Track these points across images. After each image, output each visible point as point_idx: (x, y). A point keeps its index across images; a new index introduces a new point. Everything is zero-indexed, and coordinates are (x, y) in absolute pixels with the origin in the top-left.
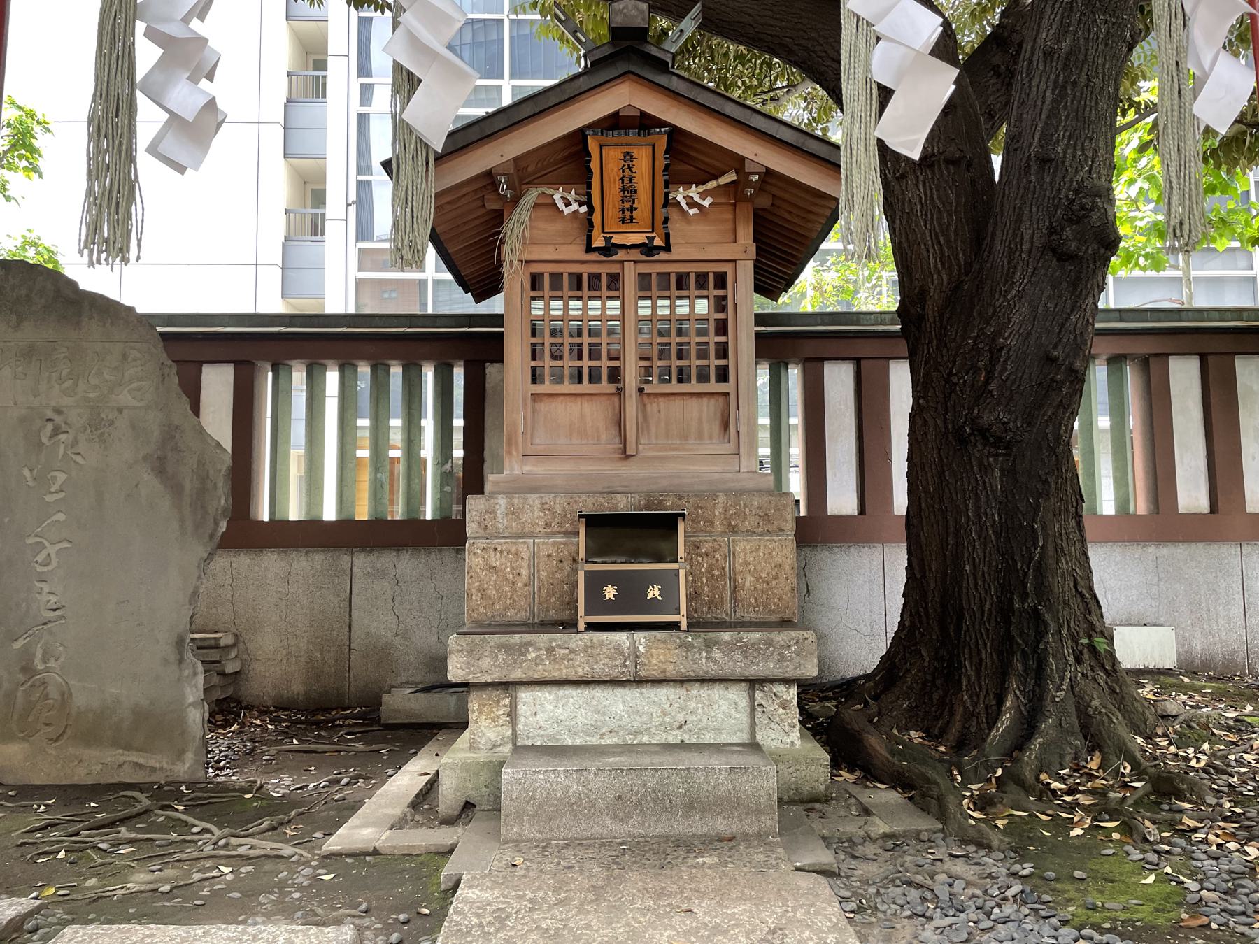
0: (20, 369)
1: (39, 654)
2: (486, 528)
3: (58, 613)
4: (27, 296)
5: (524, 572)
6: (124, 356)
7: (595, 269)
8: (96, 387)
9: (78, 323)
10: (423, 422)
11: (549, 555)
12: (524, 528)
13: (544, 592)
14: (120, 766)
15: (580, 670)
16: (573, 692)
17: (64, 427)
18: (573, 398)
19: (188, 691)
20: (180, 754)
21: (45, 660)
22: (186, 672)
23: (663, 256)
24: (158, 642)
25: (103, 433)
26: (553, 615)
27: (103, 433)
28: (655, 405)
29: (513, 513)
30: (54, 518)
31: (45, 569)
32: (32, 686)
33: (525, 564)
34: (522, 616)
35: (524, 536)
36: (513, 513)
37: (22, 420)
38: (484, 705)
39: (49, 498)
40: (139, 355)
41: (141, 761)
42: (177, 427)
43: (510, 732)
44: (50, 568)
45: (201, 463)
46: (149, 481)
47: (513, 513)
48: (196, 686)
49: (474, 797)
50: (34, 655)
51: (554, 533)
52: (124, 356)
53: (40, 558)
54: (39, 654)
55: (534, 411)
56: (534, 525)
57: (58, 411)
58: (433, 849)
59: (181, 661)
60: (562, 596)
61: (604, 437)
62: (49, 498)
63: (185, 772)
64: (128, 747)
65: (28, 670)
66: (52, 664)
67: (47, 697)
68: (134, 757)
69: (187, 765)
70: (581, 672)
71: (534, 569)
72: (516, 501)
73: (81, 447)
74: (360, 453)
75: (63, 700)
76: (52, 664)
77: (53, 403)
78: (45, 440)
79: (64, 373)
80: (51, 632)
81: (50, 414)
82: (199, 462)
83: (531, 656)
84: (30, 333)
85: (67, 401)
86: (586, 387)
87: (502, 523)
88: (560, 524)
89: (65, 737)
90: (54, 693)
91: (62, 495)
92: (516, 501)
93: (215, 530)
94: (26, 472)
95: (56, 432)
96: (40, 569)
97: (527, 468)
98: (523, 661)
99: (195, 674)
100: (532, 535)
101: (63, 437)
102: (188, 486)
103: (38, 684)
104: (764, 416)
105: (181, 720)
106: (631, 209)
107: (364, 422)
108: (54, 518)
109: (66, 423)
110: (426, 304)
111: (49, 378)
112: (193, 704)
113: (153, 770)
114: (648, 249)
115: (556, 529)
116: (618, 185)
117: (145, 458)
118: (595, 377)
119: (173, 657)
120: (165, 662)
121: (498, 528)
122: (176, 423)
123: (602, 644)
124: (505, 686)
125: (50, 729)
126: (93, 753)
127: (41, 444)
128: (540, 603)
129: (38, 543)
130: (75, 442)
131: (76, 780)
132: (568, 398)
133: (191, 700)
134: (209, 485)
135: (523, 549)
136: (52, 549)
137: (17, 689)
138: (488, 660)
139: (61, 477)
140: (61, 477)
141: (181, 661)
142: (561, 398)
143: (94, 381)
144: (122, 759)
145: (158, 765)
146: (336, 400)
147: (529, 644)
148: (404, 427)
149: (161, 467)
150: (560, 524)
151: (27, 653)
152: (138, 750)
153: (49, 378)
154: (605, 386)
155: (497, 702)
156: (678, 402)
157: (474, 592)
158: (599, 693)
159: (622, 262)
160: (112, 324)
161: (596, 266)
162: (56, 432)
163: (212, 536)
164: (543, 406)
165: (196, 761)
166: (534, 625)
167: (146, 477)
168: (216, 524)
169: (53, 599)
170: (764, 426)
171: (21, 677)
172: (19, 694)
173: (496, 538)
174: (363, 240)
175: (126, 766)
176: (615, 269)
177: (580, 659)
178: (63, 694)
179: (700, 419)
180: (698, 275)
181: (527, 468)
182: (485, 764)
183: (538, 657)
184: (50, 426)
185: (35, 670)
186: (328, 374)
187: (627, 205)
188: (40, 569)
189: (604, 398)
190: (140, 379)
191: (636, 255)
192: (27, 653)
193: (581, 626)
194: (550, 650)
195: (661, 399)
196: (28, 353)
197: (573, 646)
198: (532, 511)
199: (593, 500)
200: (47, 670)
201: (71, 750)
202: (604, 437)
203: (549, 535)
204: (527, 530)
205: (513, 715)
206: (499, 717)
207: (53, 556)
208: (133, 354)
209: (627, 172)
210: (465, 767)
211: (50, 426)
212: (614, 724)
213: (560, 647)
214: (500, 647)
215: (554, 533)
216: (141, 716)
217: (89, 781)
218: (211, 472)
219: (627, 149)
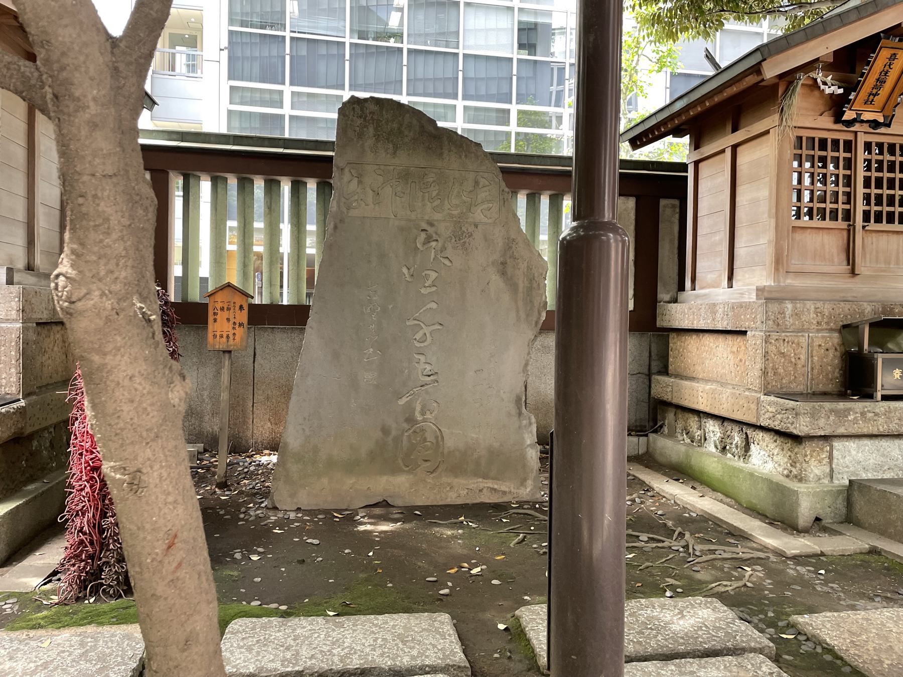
0: (399, 189)
1: (418, 408)
2: (778, 325)
3: (432, 377)
4: (399, 129)
5: (802, 357)
6: (477, 183)
7: (836, 136)
8: (457, 206)
9: (441, 154)
10: (282, 226)
11: (820, 345)
12: (803, 326)
13: (816, 371)
14: (481, 491)
15: (881, 428)
16: (866, 442)
17: (435, 237)
18: (817, 231)
19: (526, 436)
20: (523, 482)
21: (423, 413)
22: (524, 422)
23: (883, 130)
24: (503, 400)
25: (465, 243)
26: (821, 388)
27: (465, 243)
28: (870, 238)
29: (797, 314)
30: (428, 306)
31: (422, 345)
32: (415, 432)
33: (804, 351)
34: (800, 388)
35: (803, 331)
36: (797, 314)
37: (402, 229)
38: (814, 451)
39: (423, 291)
40: (487, 183)
41: (496, 487)
42: (514, 240)
43: (828, 470)
44: (425, 344)
45: (529, 268)
46: (496, 280)
47: (796, 315)
48: (531, 432)
49: (821, 513)
50: (415, 409)
51: (822, 330)
52: (477, 183)
53: (418, 336)
54: (418, 408)
55: (792, 239)
56: (810, 323)
57: (431, 224)
58: (858, 551)
59: (520, 414)
60: (827, 374)
61: (836, 260)
62: (423, 291)
63: (527, 495)
64: (486, 477)
65: (411, 420)
66: (428, 416)
67: (425, 440)
68: (490, 484)
69: (528, 490)
70: (882, 429)
71: (810, 355)
72: (798, 305)
73: (449, 253)
74: (229, 247)
75: (437, 441)
76: (428, 416)
77: (426, 218)
78: (419, 246)
79: (434, 194)
80: (427, 392)
81: (424, 225)
82: (528, 267)
83: (851, 418)
84: (403, 160)
85: (437, 216)
86: (828, 223)
87: (789, 321)
88: (827, 323)
89: (439, 470)
90: (430, 437)
91: (434, 289)
92: (798, 305)
93: (539, 318)
94: (405, 270)
95: (429, 240)
96: (418, 345)
97: (789, 281)
98: (845, 421)
99: (530, 424)
100: (808, 330)
101: (434, 244)
102: (521, 286)
103: (418, 430)
104: (312, 224)
105: (523, 457)
106: (875, 95)
107: (232, 223)
108: (428, 306)
109: (436, 233)
110: (510, 147)
111: (423, 197)
112: (531, 446)
113: (504, 493)
114: (875, 124)
115: (825, 326)
116: (877, 76)
117: (493, 263)
118: (834, 215)
119: (514, 411)
120: (509, 415)
121: (786, 325)
122: (513, 237)
123: (896, 409)
124: (825, 438)
125: (428, 464)
126: (461, 481)
127: (417, 248)
128: (812, 379)
129: (416, 325)
130: (444, 249)
131: (449, 501)
132: (813, 231)
133: (528, 442)
134: (535, 285)
135: (802, 340)
136: (427, 330)
137: (402, 434)
138: (823, 420)
139: (433, 275)
140: (433, 275)
141: (520, 414)
142: (809, 230)
143: (455, 201)
144: (481, 486)
145: (507, 490)
146: (209, 205)
147: (849, 410)
148: (239, 227)
149: (503, 269)
150: (827, 323)
151: (409, 407)
152: (493, 479)
153: (423, 197)
154: (841, 224)
155: (822, 449)
156: (884, 237)
157: (770, 370)
158: (884, 443)
159: (856, 133)
160: (466, 156)
161: (838, 133)
162: (429, 240)
163: (537, 323)
164: (798, 236)
165: (535, 487)
166: (808, 394)
167: (494, 277)
168: (540, 314)
169: (428, 367)
170: (259, 229)
171: (406, 426)
172: (405, 438)
173: (784, 332)
174: (344, 85)
175: (485, 490)
176: (850, 137)
177: (882, 420)
178: (437, 437)
179: (898, 250)
180: (845, 142)
181: (789, 281)
182: (828, 492)
183: (855, 418)
184: (423, 235)
185: (417, 421)
186: (542, 197)
187: (874, 91)
188: (418, 345)
189: (837, 231)
190: (489, 201)
191: (866, 128)
192: (409, 407)
193: (879, 397)
194: (863, 414)
195: (874, 234)
196: (405, 176)
197: (877, 411)
198: (809, 313)
199: (849, 307)
200: (424, 420)
201: (445, 479)
202: (836, 260)
203: (818, 331)
204: (805, 327)
205: (831, 457)
206: (823, 459)
207: (428, 335)
208: (483, 182)
209: (887, 67)
210: (815, 494)
211: (423, 235)
212: (892, 463)
213: (869, 411)
214: (831, 411)
215: (822, 330)
216: (494, 455)
217: (459, 502)
218: (536, 275)
219: (893, 51)
